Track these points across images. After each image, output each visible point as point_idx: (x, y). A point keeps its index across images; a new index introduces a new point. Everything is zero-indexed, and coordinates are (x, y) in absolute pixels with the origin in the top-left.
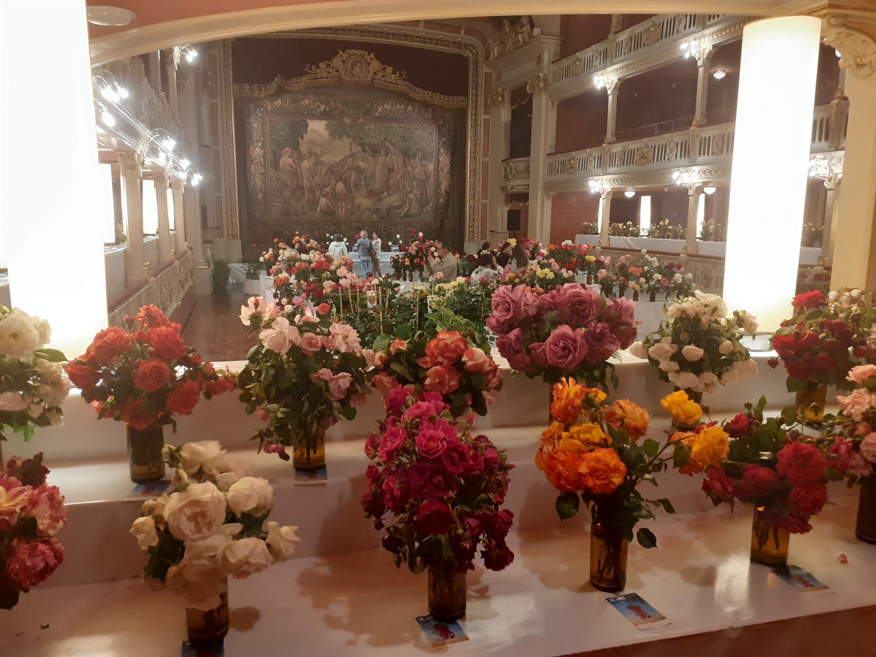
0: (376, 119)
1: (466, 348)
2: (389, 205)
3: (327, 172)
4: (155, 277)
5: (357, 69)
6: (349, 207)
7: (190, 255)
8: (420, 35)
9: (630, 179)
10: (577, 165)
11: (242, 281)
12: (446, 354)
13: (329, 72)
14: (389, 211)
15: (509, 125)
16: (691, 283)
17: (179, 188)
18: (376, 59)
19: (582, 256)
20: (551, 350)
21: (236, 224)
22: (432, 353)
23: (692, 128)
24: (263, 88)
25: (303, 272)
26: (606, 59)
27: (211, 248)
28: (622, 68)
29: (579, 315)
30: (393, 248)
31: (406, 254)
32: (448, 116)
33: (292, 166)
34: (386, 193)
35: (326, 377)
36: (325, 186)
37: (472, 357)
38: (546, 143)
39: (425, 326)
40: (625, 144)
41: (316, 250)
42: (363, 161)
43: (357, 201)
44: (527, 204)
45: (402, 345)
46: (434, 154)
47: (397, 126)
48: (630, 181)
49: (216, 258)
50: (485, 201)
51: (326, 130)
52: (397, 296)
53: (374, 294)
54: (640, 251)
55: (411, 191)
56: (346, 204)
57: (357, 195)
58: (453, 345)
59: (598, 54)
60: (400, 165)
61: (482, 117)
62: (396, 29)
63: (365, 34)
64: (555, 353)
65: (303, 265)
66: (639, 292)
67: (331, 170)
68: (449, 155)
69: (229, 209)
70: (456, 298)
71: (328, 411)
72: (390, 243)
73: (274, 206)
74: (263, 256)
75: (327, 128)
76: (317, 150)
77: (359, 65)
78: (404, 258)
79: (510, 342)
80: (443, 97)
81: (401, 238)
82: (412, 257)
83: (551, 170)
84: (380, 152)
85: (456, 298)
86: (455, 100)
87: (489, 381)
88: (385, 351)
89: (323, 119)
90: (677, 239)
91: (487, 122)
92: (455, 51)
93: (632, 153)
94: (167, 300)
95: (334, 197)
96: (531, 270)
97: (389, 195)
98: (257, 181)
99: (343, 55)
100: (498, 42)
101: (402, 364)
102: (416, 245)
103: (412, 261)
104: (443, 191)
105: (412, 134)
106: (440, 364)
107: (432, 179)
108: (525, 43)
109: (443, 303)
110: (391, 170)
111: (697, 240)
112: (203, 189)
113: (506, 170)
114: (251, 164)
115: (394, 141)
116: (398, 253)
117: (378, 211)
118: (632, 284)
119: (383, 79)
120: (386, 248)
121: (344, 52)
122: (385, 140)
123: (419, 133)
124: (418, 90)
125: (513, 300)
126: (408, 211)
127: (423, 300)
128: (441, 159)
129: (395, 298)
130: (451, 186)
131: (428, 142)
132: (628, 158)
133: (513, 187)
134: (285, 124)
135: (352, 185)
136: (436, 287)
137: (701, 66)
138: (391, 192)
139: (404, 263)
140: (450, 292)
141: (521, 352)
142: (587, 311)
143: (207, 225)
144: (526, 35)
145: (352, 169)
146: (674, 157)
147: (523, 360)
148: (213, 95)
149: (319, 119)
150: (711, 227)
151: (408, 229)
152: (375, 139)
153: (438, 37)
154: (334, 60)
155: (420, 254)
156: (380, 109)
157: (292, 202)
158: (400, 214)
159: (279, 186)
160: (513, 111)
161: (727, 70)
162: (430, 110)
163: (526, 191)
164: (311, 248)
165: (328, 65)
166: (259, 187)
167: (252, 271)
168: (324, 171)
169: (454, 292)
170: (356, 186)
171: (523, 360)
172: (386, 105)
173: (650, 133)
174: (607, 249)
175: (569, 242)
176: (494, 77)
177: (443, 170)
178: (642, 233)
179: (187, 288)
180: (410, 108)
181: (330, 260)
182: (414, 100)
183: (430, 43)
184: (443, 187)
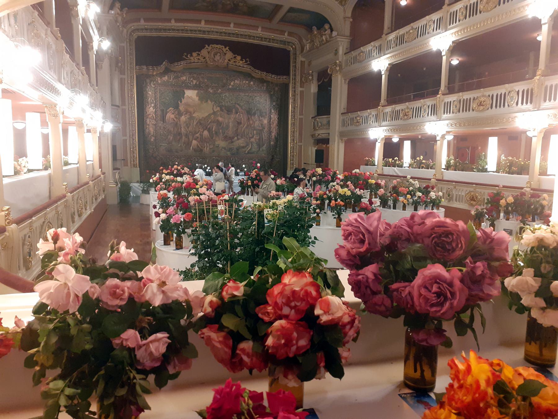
0: (229, 90)
1: (320, 295)
3: (197, 123)
4: (71, 193)
5: (217, 58)
6: (211, 147)
7: (103, 178)
8: (258, 36)
9: (396, 130)
10: (361, 120)
11: (139, 195)
12: (293, 304)
13: (199, 59)
14: (238, 149)
15: (316, 95)
16: (441, 199)
17: (95, 132)
18: (230, 51)
19: (366, 179)
20: (420, 295)
21: (136, 157)
22: (276, 303)
23: (439, 96)
25: (177, 190)
26: (381, 51)
27: (119, 173)
29: (444, 248)
30: (241, 174)
31: (249, 178)
32: (276, 89)
33: (174, 120)
34: (236, 138)
35: (131, 344)
37: (327, 308)
38: (340, 107)
39: (263, 232)
40: (394, 106)
41: (188, 174)
42: (221, 117)
43: (217, 143)
44: (328, 146)
45: (237, 289)
46: (268, 113)
47: (243, 94)
48: (397, 131)
49: (122, 180)
50: (300, 144)
52: (241, 208)
53: (223, 208)
54: (406, 177)
55: (252, 137)
57: (217, 139)
58: (302, 292)
59: (375, 48)
61: (299, 89)
62: (243, 31)
63: (223, 34)
64: (427, 300)
65: (177, 185)
66: (406, 204)
67: (200, 123)
68: (277, 114)
69: (132, 147)
70: (286, 211)
71: (131, 398)
74: (152, 178)
76: (191, 110)
77: (219, 54)
78: (248, 181)
79: (367, 281)
80: (273, 76)
81: (245, 167)
82: (252, 180)
83: (344, 123)
84: (232, 111)
85: (286, 211)
86: (281, 78)
87: (346, 334)
88: (217, 294)
89: (195, 89)
90: (428, 169)
91: (302, 92)
92: (282, 46)
93: (398, 112)
94: (82, 209)
95: (202, 140)
96: (335, 189)
97: (238, 139)
98: (150, 129)
99: (208, 48)
100: (309, 41)
101: (237, 315)
102: (256, 172)
103: (252, 182)
104: (273, 137)
105: (253, 99)
106: (286, 317)
108: (327, 41)
109: (276, 215)
110: (239, 123)
111: (443, 170)
112: (114, 135)
113: (314, 123)
114: (147, 118)
115: (242, 104)
116: (243, 177)
117: (230, 150)
118: (401, 199)
119: (234, 64)
120: (237, 174)
121: (209, 46)
122: (235, 104)
123: (258, 100)
125: (367, 230)
126: (250, 149)
127: (261, 214)
128: (272, 116)
129: (240, 210)
130: (279, 134)
131: (264, 105)
132: (396, 116)
133: (319, 135)
134: (169, 93)
135: (214, 132)
136: (271, 203)
137: (444, 55)
138: (239, 137)
139: (247, 184)
140: (281, 206)
141: (380, 292)
142: (454, 245)
143: (116, 158)
144: (328, 37)
145: (214, 122)
146: (427, 115)
147: (382, 303)
148: (122, 72)
149: (192, 89)
150: (452, 161)
151: (251, 161)
153: (270, 37)
154: (202, 51)
155: (258, 178)
156: (232, 84)
157: (174, 143)
160: (319, 86)
161: (460, 59)
162: (265, 84)
163: (327, 137)
164: (185, 173)
165: (199, 55)
166: (152, 133)
167: (146, 189)
168: (195, 123)
169: (285, 206)
170: (216, 133)
171: (382, 303)
172: (236, 81)
173: (409, 100)
174: (382, 176)
175: (357, 171)
177: (273, 123)
178: (405, 165)
179: (99, 200)
180: (252, 83)
181: (196, 182)
182: (254, 78)
183: (266, 41)
184: (273, 134)
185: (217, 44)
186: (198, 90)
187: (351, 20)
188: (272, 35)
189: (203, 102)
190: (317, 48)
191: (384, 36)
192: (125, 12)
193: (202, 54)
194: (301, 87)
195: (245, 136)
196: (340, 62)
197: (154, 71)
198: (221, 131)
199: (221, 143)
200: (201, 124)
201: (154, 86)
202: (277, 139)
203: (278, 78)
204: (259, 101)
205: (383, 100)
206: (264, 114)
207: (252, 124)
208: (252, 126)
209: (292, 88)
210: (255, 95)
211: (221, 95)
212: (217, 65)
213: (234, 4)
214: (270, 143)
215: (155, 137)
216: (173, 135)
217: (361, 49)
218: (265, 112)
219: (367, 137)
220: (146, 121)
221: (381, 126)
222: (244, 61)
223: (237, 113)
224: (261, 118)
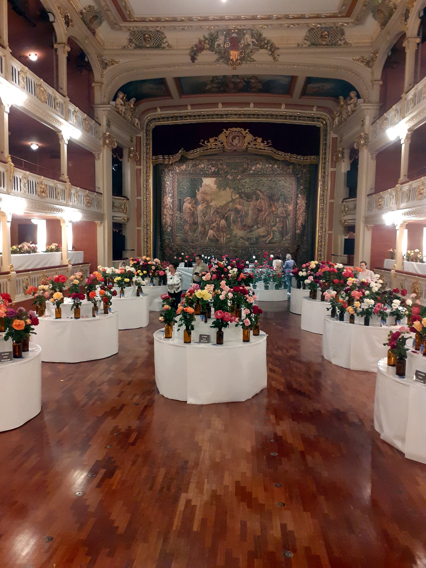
2: (257, 235)
3: (214, 212)
5: (236, 141)
6: (229, 236)
8: (281, 113)
13: (216, 145)
18: (250, 133)
21: (150, 248)
24: (171, 158)
28: (409, 120)
32: (305, 171)
33: (191, 210)
34: (256, 227)
36: (212, 222)
42: (240, 205)
43: (234, 232)
46: (293, 198)
47: (265, 179)
50: (330, 232)
51: (215, 184)
55: (275, 225)
56: (227, 234)
57: (235, 229)
60: (267, 208)
67: (217, 212)
72: (247, 262)
73: (177, 236)
75: (216, 183)
76: (208, 198)
77: (237, 138)
80: (299, 157)
84: (252, 198)
86: (308, 158)
89: (213, 177)
95: (219, 229)
97: (258, 228)
104: (300, 225)
105: (277, 184)
107: (291, 216)
108: (353, 111)
110: (260, 211)
115: (263, 190)
117: (249, 239)
119: (254, 147)
122: (256, 190)
123: (282, 184)
124: (280, 153)
126: (272, 239)
128: (298, 201)
130: (306, 221)
131: (289, 190)
135: (231, 221)
138: (259, 226)
149: (210, 177)
152: (249, 189)
153: (296, 114)
154: (220, 136)
157: (189, 233)
158: (266, 241)
159: (182, 223)
162: (291, 167)
165: (216, 140)
168: (212, 212)
170: (234, 222)
172: (258, 166)
176: (339, 139)
177: (300, 209)
180: (276, 166)
182: (279, 160)
185: (236, 127)
186: (216, 177)
187: (381, 83)
188: (298, 112)
189: (222, 190)
190: (345, 120)
191: (403, 95)
192: (133, 102)
193: (220, 139)
194: (332, 167)
195: (265, 224)
196: (366, 134)
197: (167, 160)
198: (239, 219)
199: (239, 232)
200: (218, 213)
201: (172, 176)
202: (303, 226)
203: (305, 158)
204: (283, 185)
205: (402, 178)
206: (289, 200)
207: (275, 211)
208: (275, 213)
209: (321, 169)
210: (280, 179)
211: (241, 182)
212: (235, 150)
213: (245, 82)
214: (295, 230)
215: (172, 227)
216: (189, 225)
217: (385, 116)
218: (291, 197)
219: (379, 223)
220: (163, 211)
221: (398, 209)
222: (266, 143)
223: (258, 200)
224: (285, 204)
